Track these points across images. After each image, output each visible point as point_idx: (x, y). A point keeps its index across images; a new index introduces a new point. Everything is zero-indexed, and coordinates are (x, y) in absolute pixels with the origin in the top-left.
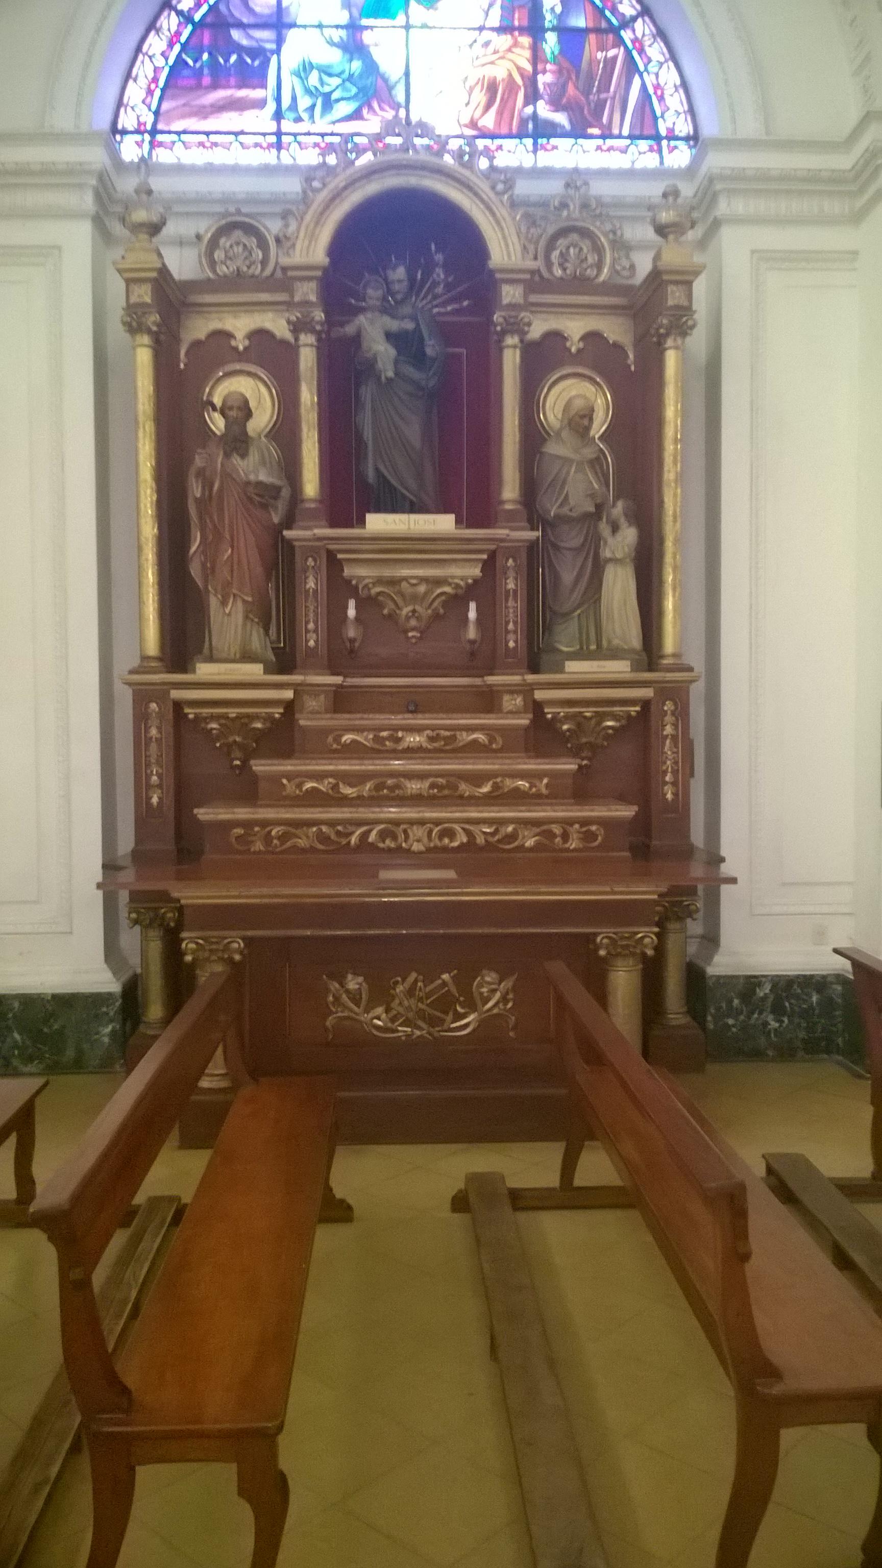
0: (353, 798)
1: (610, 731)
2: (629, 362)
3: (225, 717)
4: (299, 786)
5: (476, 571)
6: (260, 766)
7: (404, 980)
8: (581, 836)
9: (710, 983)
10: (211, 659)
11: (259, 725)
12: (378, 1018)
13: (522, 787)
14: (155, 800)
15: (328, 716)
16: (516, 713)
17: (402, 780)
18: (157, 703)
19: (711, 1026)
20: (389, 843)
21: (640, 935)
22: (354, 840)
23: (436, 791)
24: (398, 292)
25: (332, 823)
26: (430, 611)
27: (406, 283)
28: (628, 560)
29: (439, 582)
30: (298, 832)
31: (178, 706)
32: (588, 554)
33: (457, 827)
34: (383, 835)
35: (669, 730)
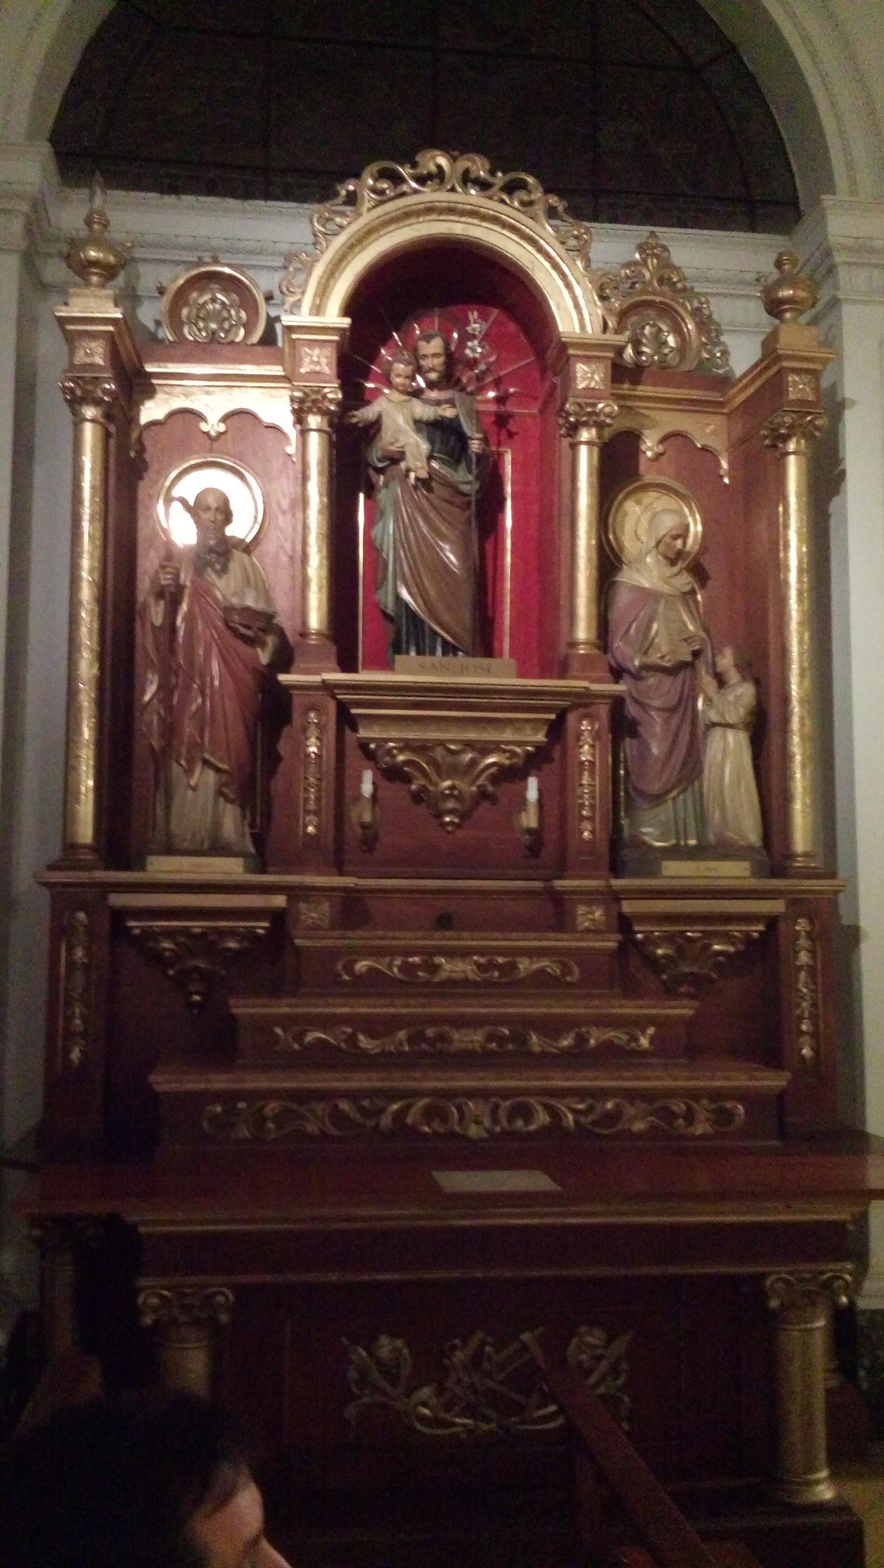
0: (375, 1055)
1: (721, 959)
2: (722, 472)
3: (186, 932)
4: (299, 1037)
5: (541, 737)
6: (244, 1008)
7: (465, 1341)
8: (710, 1115)
9: (862, 1321)
10: (170, 850)
11: (232, 945)
12: (424, 1402)
13: (616, 1041)
14: (75, 1055)
15: (336, 933)
16: (595, 932)
17: (447, 1028)
18: (87, 913)
19: (865, 1386)
20: (437, 1126)
21: (826, 1276)
22: (386, 1121)
23: (494, 1045)
24: (432, 370)
25: (354, 1096)
26: (474, 789)
27: (442, 359)
28: (742, 725)
29: (485, 749)
30: (302, 1110)
31: (119, 915)
32: (684, 714)
33: (532, 1101)
34: (429, 1114)
35: (804, 957)
